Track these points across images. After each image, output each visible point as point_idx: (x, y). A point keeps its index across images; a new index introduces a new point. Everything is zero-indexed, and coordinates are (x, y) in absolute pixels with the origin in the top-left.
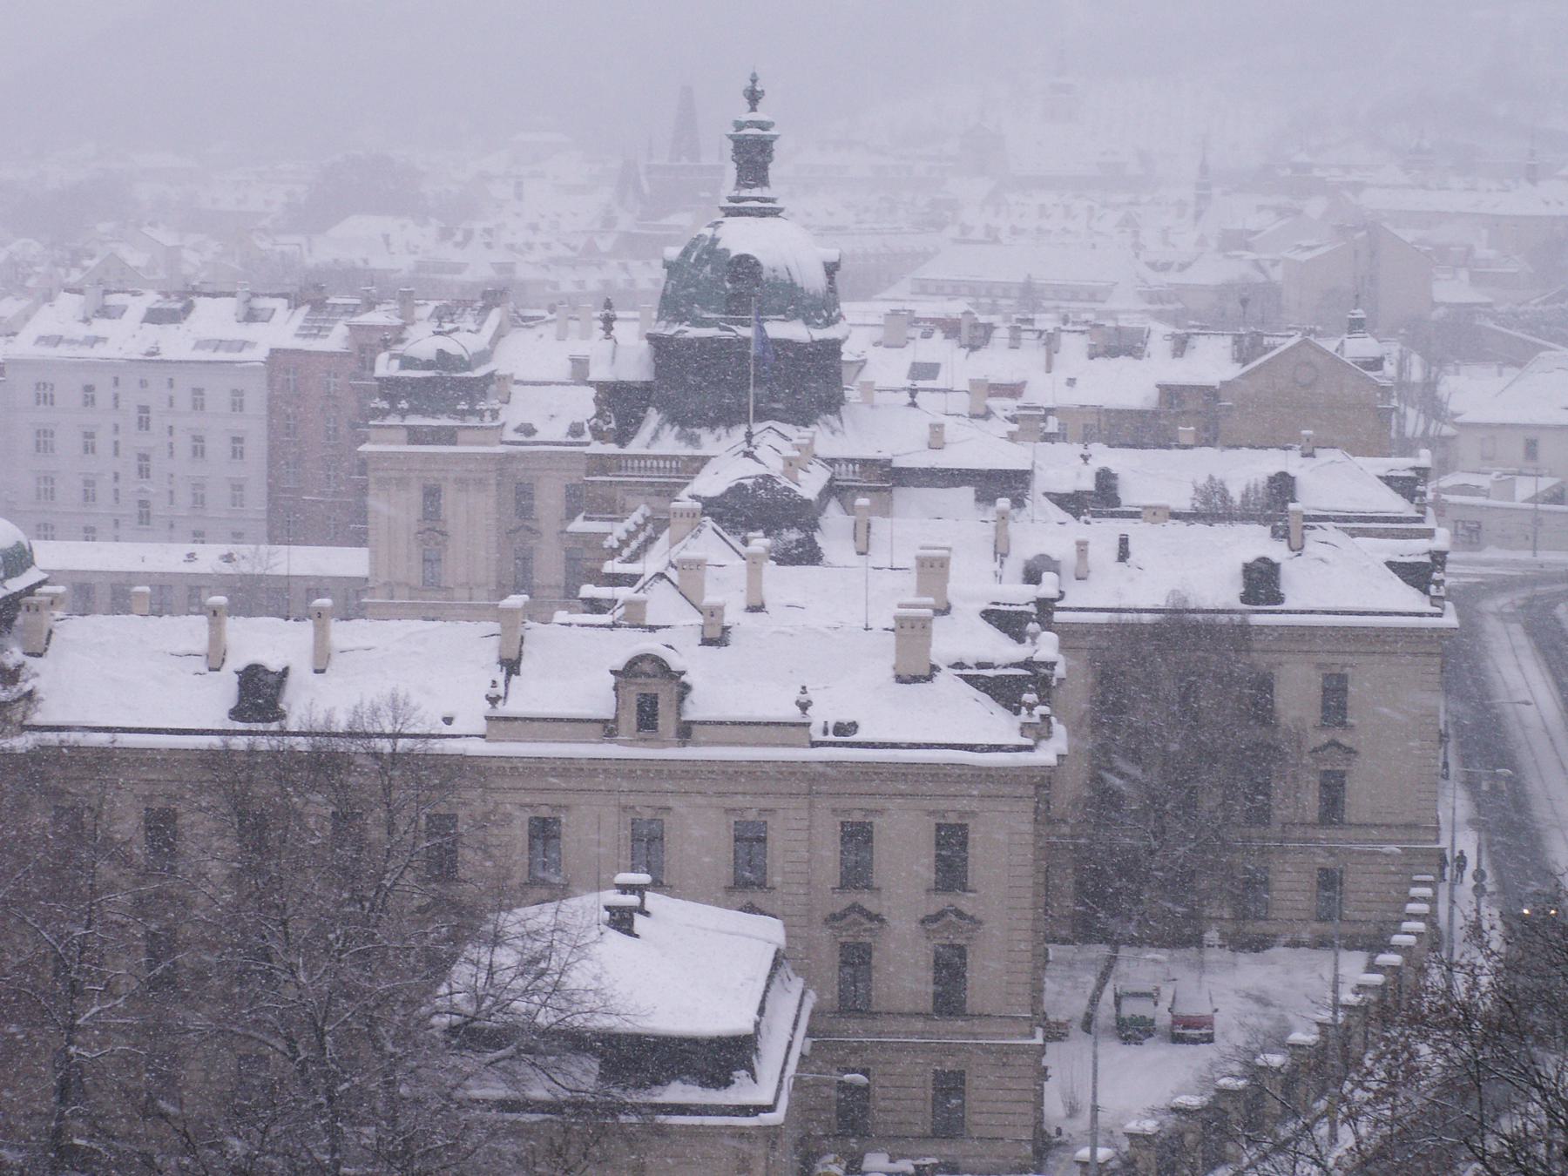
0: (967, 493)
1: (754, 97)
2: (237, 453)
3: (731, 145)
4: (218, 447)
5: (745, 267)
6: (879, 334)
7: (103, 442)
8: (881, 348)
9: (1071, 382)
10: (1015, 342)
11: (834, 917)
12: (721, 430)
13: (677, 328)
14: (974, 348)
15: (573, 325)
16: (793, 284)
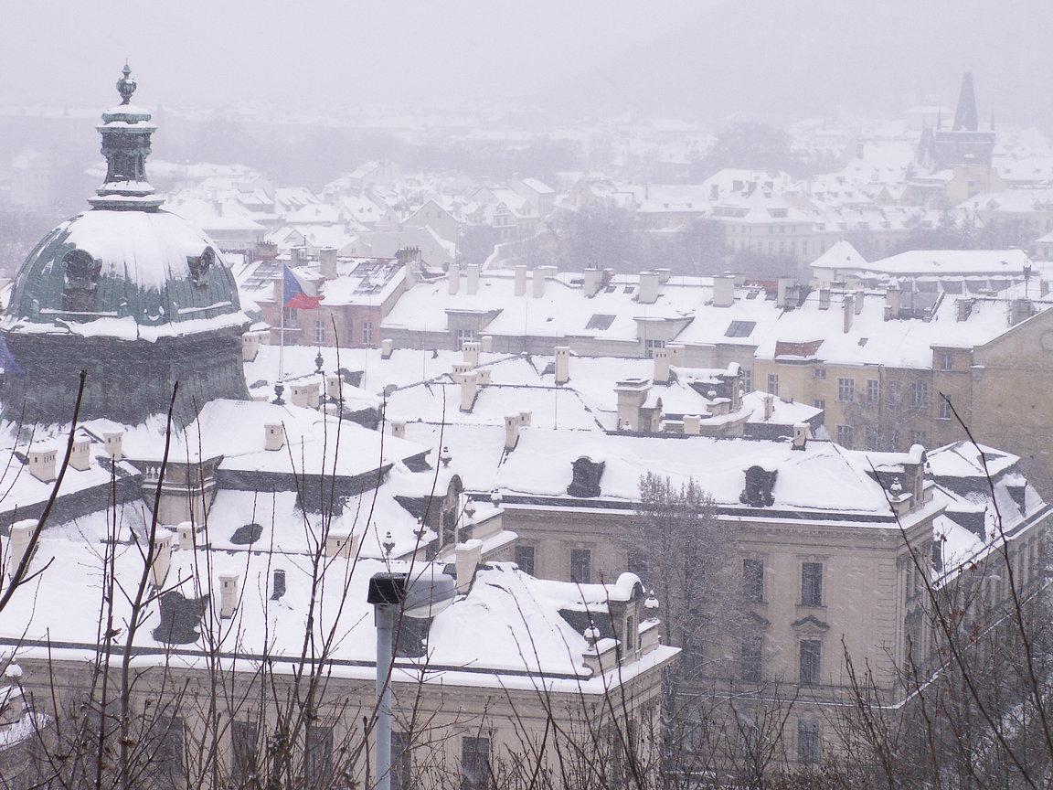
0: (289, 498)
1: (126, 91)
3: (100, 138)
5: (80, 264)
8: (710, 307)
9: (863, 342)
10: (824, 305)
13: (16, 323)
14: (787, 309)
15: (463, 281)
16: (128, 280)
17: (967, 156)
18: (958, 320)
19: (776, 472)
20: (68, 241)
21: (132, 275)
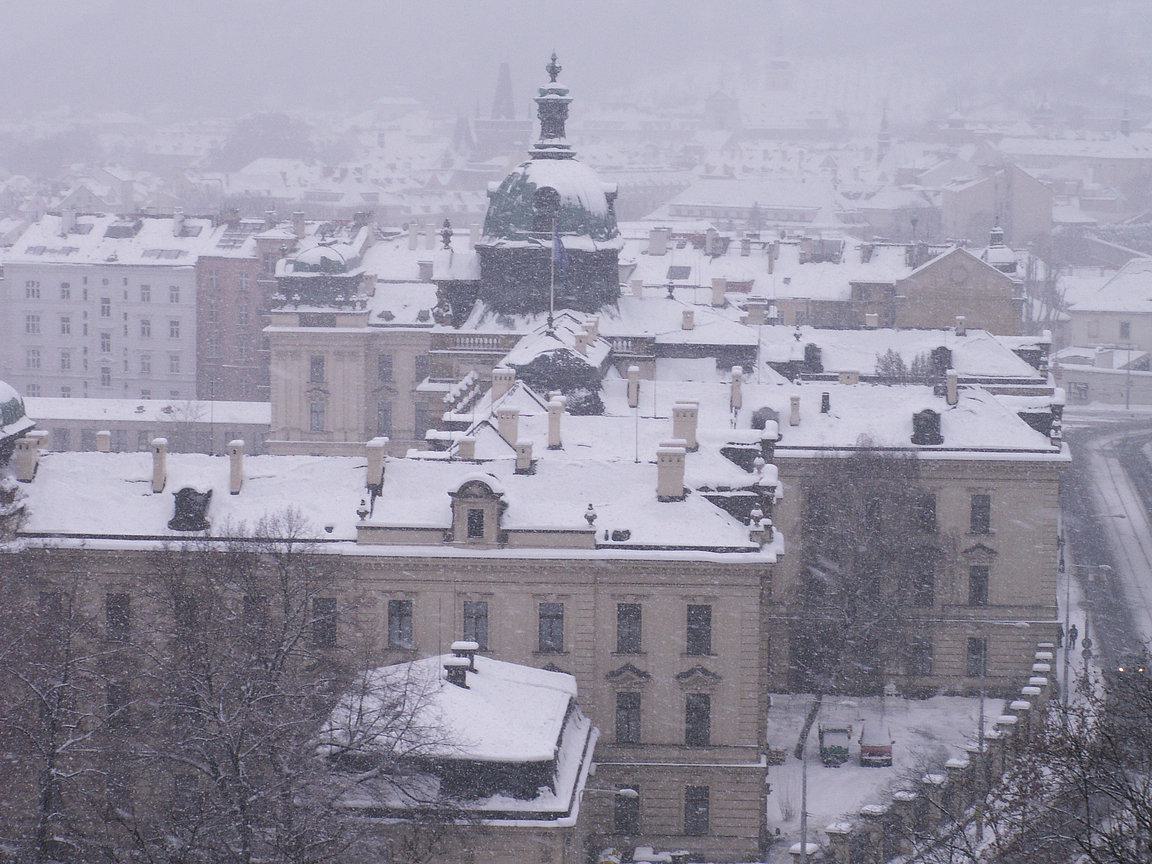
0: (710, 363)
1: (554, 72)
2: (174, 333)
4: (160, 328)
5: (547, 197)
6: (646, 245)
7: (76, 325)
11: (613, 674)
12: (530, 316)
13: (497, 241)
14: (716, 256)
16: (583, 209)
17: (516, 143)
18: (863, 261)
19: (210, 493)
20: (529, 181)
21: (585, 204)
